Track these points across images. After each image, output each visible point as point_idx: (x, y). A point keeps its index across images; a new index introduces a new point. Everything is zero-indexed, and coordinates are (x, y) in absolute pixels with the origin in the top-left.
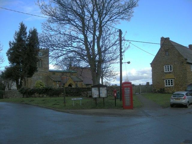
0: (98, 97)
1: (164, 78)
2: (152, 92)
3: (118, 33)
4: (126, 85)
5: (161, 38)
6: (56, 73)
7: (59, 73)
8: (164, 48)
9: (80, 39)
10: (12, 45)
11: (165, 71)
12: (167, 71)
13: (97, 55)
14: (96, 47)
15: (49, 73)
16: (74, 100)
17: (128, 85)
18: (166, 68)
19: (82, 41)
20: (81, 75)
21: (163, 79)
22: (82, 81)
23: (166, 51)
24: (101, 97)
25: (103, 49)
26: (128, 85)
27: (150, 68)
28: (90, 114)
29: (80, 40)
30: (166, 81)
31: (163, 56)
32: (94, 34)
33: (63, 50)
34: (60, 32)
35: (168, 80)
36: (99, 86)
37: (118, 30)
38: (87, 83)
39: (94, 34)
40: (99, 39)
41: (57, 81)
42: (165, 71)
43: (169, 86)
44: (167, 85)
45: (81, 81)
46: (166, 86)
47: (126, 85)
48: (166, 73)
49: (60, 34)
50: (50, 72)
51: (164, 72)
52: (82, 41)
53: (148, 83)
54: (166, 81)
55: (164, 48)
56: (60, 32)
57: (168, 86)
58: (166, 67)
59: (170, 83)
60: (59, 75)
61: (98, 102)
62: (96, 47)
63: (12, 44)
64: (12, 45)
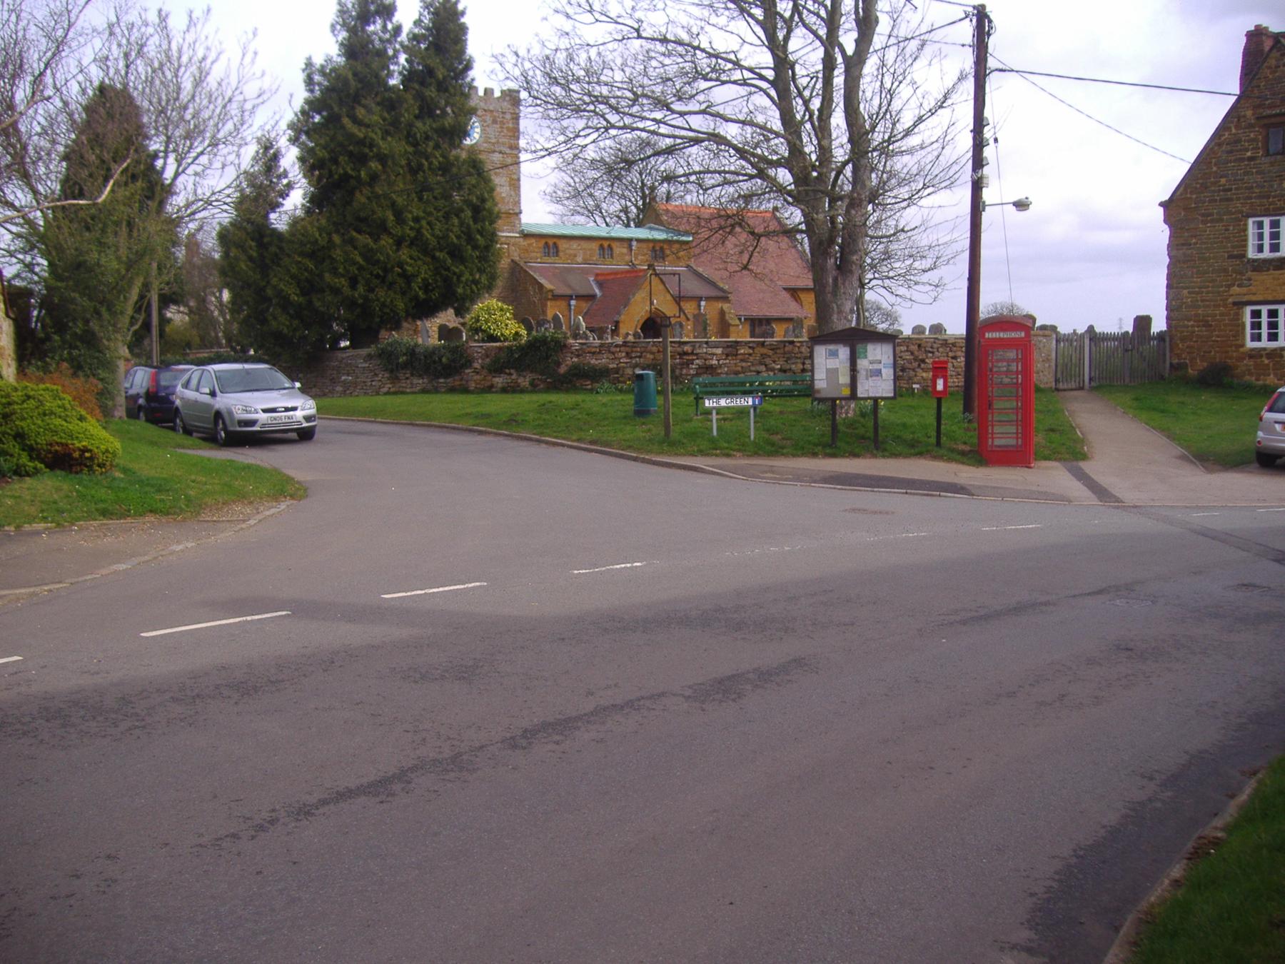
0: (846, 392)
1: (1245, 299)
2: (1162, 378)
3: (966, 31)
4: (1002, 335)
5: (1250, 35)
6: (563, 245)
7: (585, 244)
8: (1259, 106)
9: (751, 70)
10: (317, 78)
11: (1251, 254)
12: (1266, 254)
13: (845, 164)
14: (838, 120)
15: (523, 243)
16: (719, 410)
17: (1013, 335)
18: (1260, 237)
19: (762, 78)
20: (745, 267)
21: (1235, 304)
22: (725, 299)
23: (1267, 126)
24: (859, 395)
25: (877, 138)
26: (1013, 335)
27: (1162, 234)
28: (798, 477)
29: (747, 74)
30: (1256, 314)
31: (1251, 159)
32: (831, 42)
33: (648, 132)
34: (637, 31)
35: (1264, 309)
36: (858, 337)
37: (971, 9)
38: (756, 312)
39: (831, 42)
40: (854, 64)
41: (571, 297)
42: (1251, 254)
43: (1273, 345)
44: (1257, 338)
45: (717, 299)
46: (1250, 344)
47: (1002, 335)
48: (1260, 266)
49: (639, 37)
50: (526, 236)
51: (1244, 256)
52: (762, 78)
53: (1143, 323)
54: (1256, 314)
55: (1259, 106)
56: (637, 31)
57: (1264, 343)
58: (1260, 225)
59: (1264, 331)
60: (579, 259)
61: (841, 416)
62: (838, 120)
63: (322, 71)
64: (317, 78)
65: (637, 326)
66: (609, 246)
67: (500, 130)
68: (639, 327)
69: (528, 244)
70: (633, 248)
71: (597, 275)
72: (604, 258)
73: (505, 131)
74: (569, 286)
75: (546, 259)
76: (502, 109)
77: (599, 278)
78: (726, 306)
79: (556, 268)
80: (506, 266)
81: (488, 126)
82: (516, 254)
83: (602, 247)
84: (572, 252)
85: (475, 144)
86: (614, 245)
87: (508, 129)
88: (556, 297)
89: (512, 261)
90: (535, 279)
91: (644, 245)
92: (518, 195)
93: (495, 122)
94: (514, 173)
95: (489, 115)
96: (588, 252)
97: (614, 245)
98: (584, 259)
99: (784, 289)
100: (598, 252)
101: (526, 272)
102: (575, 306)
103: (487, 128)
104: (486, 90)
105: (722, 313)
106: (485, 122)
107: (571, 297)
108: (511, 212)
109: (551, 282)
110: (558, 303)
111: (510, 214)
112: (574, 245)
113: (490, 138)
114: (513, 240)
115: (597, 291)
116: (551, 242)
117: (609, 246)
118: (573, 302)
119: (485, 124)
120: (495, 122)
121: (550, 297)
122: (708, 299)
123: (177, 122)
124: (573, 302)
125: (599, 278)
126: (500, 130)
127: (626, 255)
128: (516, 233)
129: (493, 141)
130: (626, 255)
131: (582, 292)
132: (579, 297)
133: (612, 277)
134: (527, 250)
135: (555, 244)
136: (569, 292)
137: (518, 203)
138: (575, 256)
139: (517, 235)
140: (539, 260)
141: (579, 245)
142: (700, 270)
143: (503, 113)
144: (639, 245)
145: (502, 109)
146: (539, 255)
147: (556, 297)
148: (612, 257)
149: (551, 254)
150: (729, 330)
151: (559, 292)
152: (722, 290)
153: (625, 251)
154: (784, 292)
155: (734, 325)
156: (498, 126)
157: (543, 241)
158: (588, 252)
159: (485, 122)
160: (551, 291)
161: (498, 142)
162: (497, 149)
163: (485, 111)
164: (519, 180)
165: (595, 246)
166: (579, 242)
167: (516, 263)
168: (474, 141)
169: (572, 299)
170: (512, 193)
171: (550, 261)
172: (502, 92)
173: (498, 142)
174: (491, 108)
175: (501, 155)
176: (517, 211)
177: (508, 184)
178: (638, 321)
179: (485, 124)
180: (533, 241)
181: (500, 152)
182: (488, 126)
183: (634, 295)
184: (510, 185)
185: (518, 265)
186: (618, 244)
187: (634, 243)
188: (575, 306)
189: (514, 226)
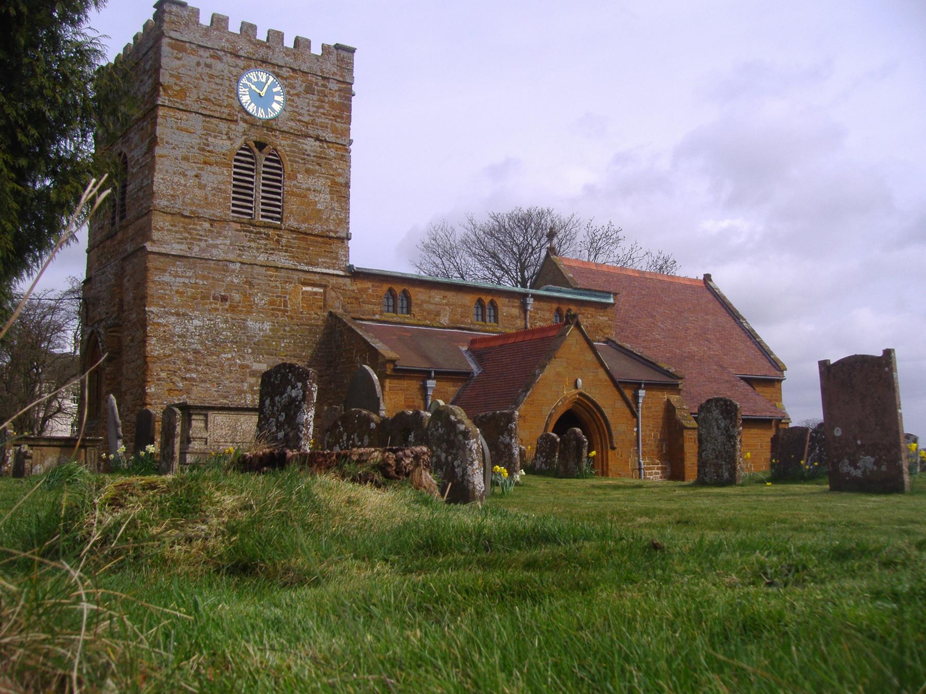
6: (418, 295)
22: (673, 387)
41: (426, 375)
65: (547, 425)
66: (492, 302)
67: (317, 104)
68: (551, 427)
69: (360, 291)
70: (529, 308)
71: (473, 342)
72: (484, 320)
73: (326, 106)
74: (426, 358)
75: (389, 316)
76: (322, 71)
77: (477, 346)
78: (674, 398)
79: (406, 330)
80: (320, 323)
81: (298, 95)
82: (337, 304)
83: (480, 301)
84: (432, 307)
85: (274, 119)
86: (500, 302)
87: (332, 104)
88: (402, 373)
89: (331, 314)
90: (364, 339)
91: (544, 305)
92: (347, 211)
93: (309, 90)
94: (340, 175)
95: (300, 77)
96: (459, 310)
97: (500, 302)
98: (451, 320)
99: (742, 378)
100: (474, 311)
101: (353, 331)
102: (434, 390)
103: (295, 98)
104: (297, 41)
105: (670, 409)
106: (294, 88)
107: (426, 375)
108: (332, 234)
109: (392, 348)
110: (405, 383)
111: (331, 238)
112: (437, 296)
113: (300, 114)
114: (333, 281)
115: (474, 367)
116: (398, 289)
117: (492, 302)
118: (431, 383)
119: (292, 92)
120: (309, 90)
121: (389, 372)
122: (650, 386)
123: (418, 465)
124: (431, 383)
125: (477, 346)
126: (317, 104)
127: (517, 317)
128: (340, 269)
129: (306, 119)
130: (517, 317)
131: (447, 367)
132: (442, 375)
133: (499, 343)
134: (357, 299)
135: (405, 292)
136: (423, 365)
137: (344, 221)
138: (438, 314)
139: (341, 273)
140: (377, 317)
141: (445, 297)
142: (628, 346)
143: (324, 78)
144: (537, 304)
145: (322, 71)
146: (377, 309)
147: (402, 373)
148: (496, 320)
149: (399, 310)
150: (682, 436)
151: (403, 364)
152: (667, 373)
153: (515, 311)
154: (743, 383)
155: (690, 428)
156: (315, 97)
157: (386, 287)
158: (459, 310)
159: (294, 88)
160: (392, 361)
161: (313, 123)
162: (311, 132)
163: (294, 70)
164: (347, 185)
165: (469, 300)
166: (443, 293)
167: (336, 317)
168: (272, 115)
169: (430, 378)
170: (336, 205)
171: (399, 320)
172: (324, 48)
173: (313, 123)
174: (304, 68)
175: (318, 143)
176: (343, 235)
177: (328, 190)
178: (551, 415)
179: (292, 92)
180: (368, 285)
181: (317, 139)
182: (298, 95)
183: (543, 367)
184: (331, 192)
185: (340, 320)
186: (505, 301)
187: (530, 301)
188: (434, 390)
189: (337, 259)
